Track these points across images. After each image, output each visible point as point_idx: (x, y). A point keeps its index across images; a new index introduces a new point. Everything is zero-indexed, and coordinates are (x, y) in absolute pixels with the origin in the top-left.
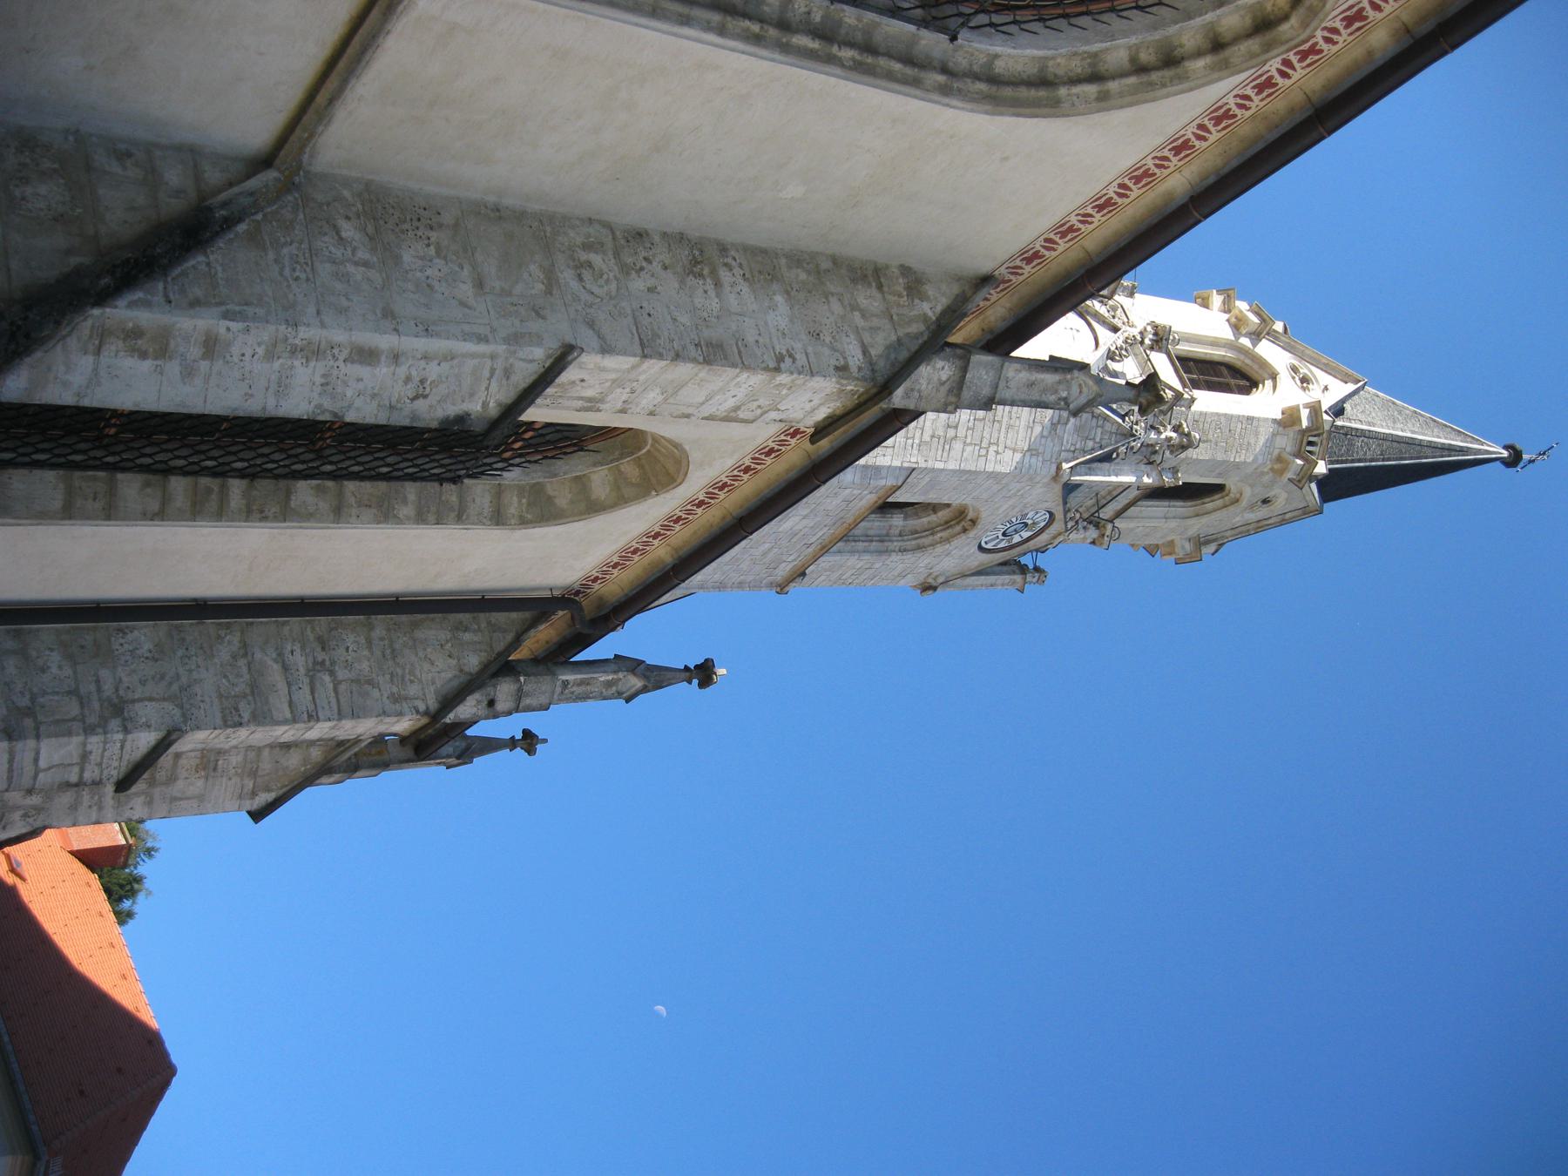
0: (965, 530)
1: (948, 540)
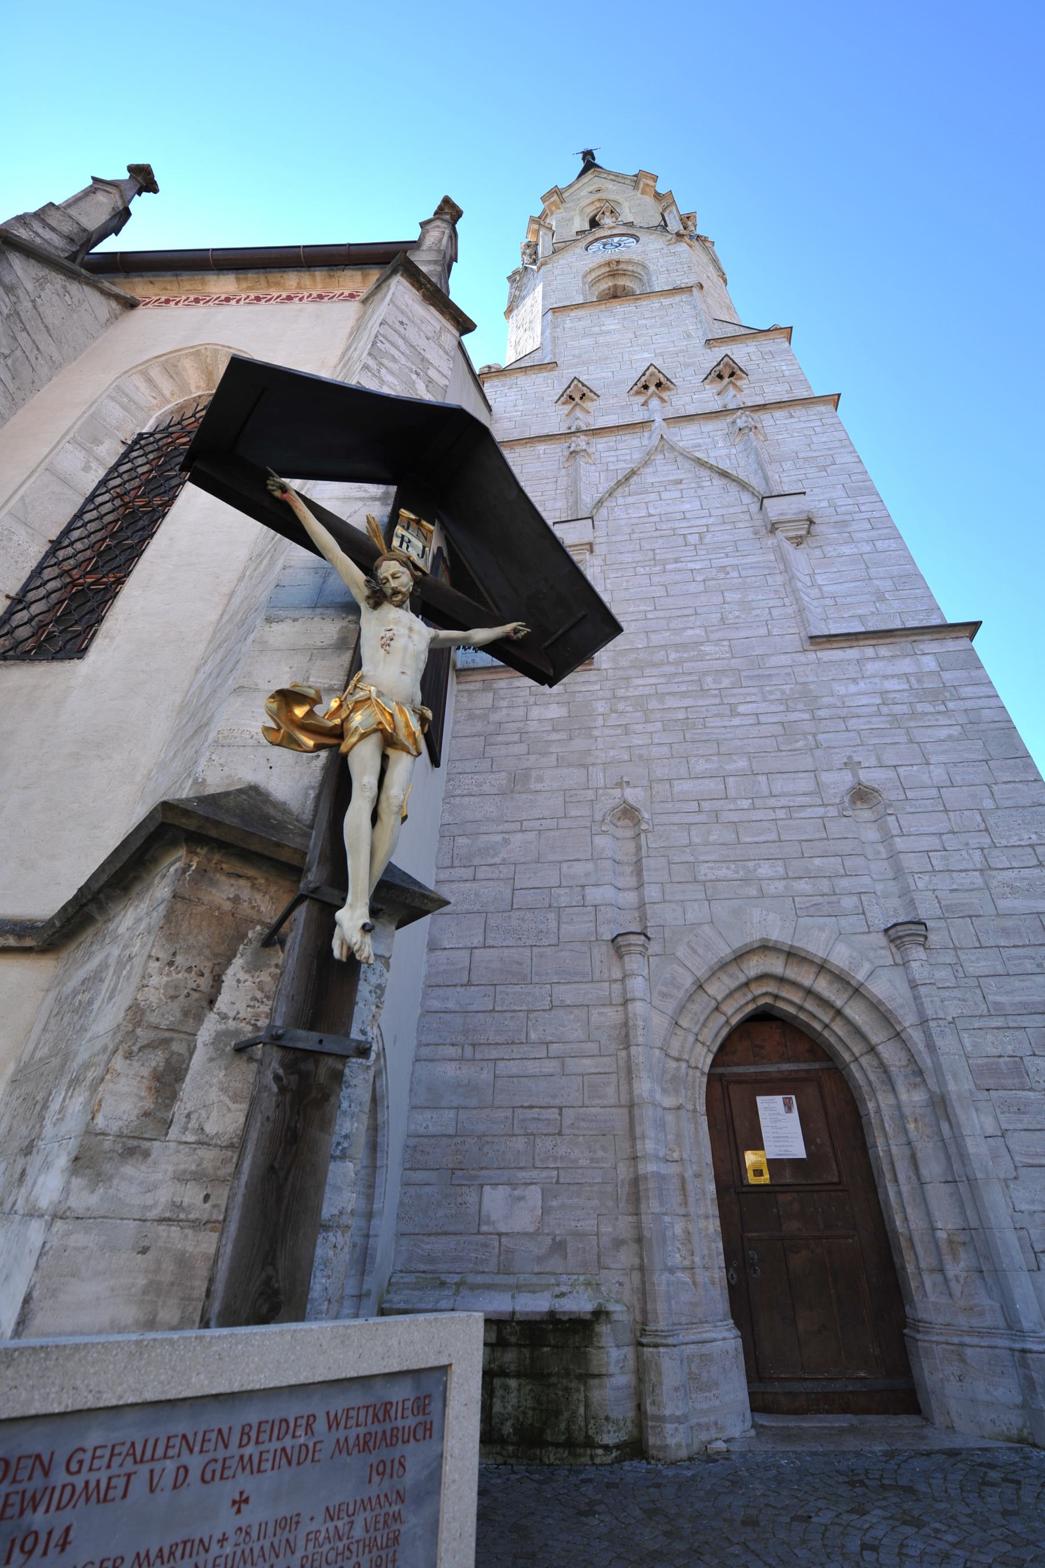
0: (618, 262)
1: (629, 262)
